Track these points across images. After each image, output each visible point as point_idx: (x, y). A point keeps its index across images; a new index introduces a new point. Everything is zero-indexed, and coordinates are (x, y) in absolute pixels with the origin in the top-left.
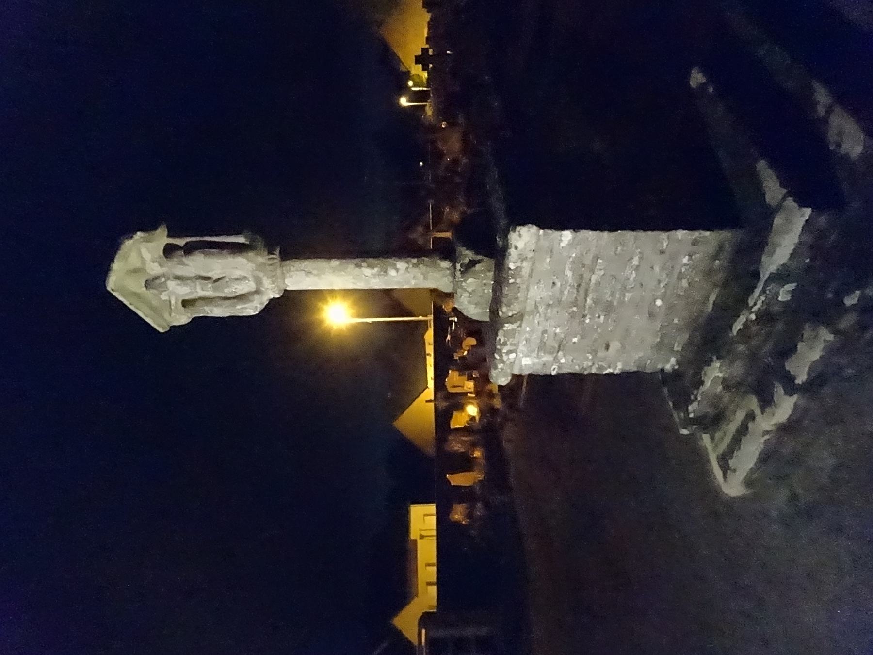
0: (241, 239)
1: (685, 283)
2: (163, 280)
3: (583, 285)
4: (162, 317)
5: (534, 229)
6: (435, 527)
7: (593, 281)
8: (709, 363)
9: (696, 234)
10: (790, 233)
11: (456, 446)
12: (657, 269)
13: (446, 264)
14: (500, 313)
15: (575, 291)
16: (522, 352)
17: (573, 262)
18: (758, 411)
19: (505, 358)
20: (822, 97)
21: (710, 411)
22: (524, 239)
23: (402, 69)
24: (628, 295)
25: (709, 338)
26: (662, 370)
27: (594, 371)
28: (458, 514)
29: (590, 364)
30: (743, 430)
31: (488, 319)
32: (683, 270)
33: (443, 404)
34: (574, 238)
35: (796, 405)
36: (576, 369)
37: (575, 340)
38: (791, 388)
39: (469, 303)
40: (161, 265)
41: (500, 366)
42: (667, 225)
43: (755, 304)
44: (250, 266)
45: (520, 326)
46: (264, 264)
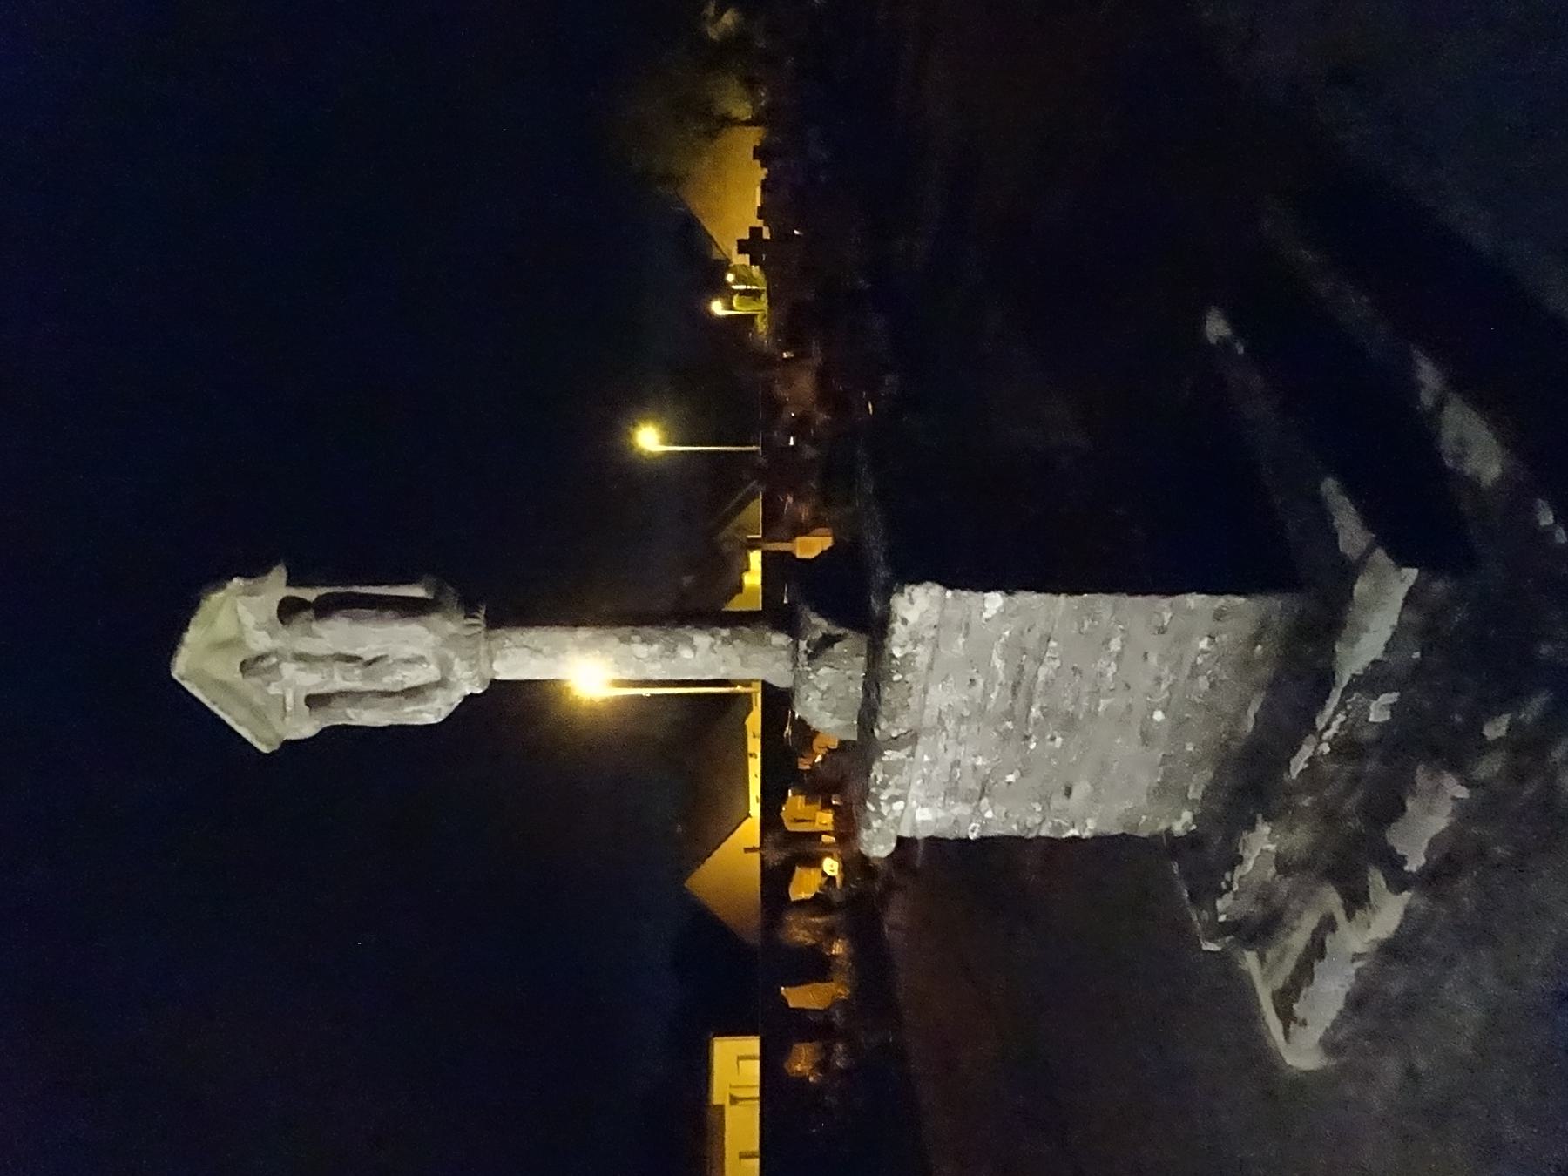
0: (417, 592)
1: (1203, 683)
2: (274, 660)
3: (1024, 684)
4: (270, 727)
5: (936, 590)
6: (757, 1081)
7: (1041, 678)
8: (1251, 826)
9: (1221, 601)
10: (1381, 613)
11: (799, 933)
12: (1153, 659)
13: (780, 639)
14: (876, 732)
15: (1009, 694)
16: (917, 798)
17: (1006, 645)
18: (1340, 916)
19: (885, 809)
20: (1429, 376)
21: (1256, 910)
22: (917, 607)
23: (716, 255)
24: (1103, 703)
25: (1249, 779)
26: (1168, 831)
27: (1044, 833)
28: (802, 1061)
29: (1038, 821)
30: (1317, 949)
31: (855, 738)
32: (1199, 661)
33: (776, 857)
34: (1005, 605)
35: (1408, 911)
36: (1014, 829)
37: (1011, 778)
38: (1399, 881)
39: (822, 708)
40: (271, 634)
41: (876, 824)
42: (1170, 586)
43: (1328, 727)
44: (431, 639)
45: (912, 754)
46: (453, 636)
